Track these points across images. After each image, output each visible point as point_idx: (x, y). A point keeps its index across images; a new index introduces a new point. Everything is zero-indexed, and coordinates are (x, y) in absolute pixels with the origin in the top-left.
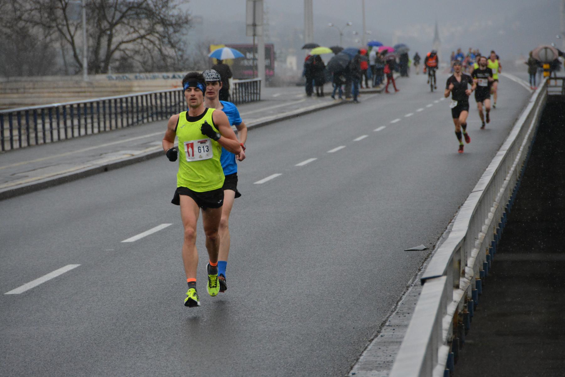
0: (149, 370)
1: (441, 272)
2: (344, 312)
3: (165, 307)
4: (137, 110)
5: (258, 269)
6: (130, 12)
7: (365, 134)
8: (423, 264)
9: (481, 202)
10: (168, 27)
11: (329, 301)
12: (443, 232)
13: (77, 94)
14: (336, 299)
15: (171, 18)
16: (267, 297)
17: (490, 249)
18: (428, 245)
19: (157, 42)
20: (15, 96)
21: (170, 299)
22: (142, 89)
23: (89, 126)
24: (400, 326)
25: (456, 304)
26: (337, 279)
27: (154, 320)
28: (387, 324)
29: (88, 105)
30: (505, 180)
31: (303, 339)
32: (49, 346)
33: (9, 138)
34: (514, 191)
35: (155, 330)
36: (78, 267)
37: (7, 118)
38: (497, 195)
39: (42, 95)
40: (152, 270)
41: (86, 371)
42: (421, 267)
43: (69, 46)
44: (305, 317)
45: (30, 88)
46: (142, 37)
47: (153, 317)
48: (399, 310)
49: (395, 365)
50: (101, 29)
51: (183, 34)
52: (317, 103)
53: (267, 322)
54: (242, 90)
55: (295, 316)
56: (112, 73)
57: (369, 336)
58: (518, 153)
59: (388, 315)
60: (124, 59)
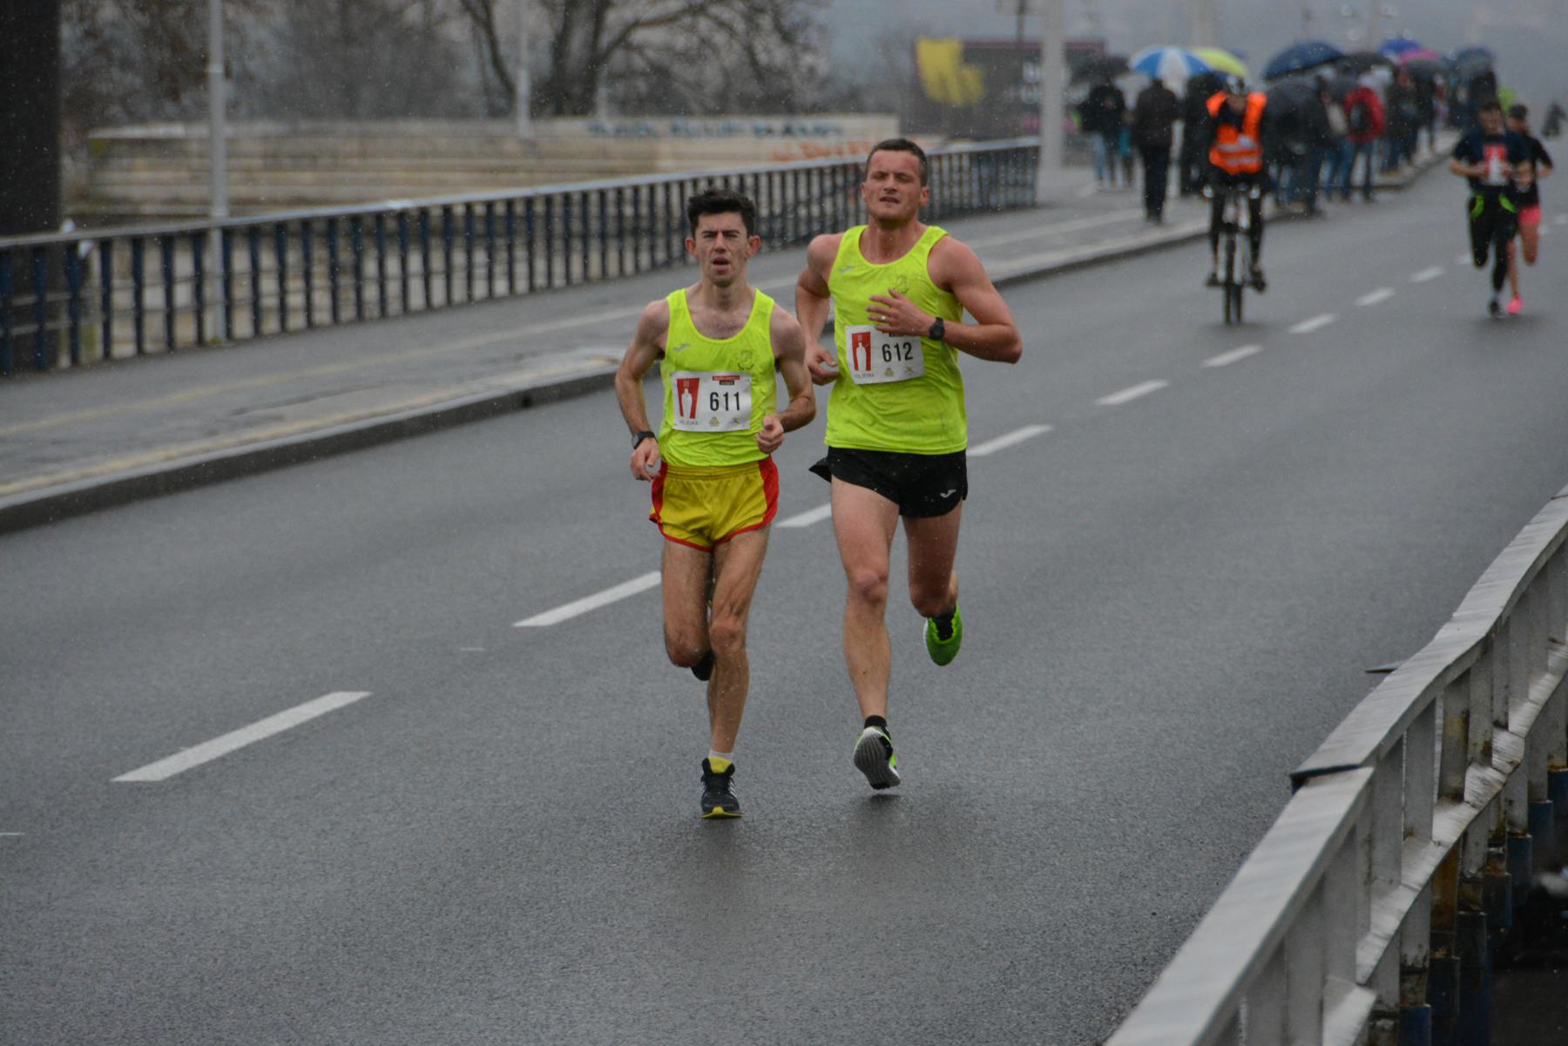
0: (487, 1033)
4: (668, 225)
20: (307, 176)
21: (613, 809)
23: (480, 272)
27: (547, 873)
29: (519, 209)
35: (541, 904)
36: (362, 701)
41: (289, 1035)
47: (547, 864)
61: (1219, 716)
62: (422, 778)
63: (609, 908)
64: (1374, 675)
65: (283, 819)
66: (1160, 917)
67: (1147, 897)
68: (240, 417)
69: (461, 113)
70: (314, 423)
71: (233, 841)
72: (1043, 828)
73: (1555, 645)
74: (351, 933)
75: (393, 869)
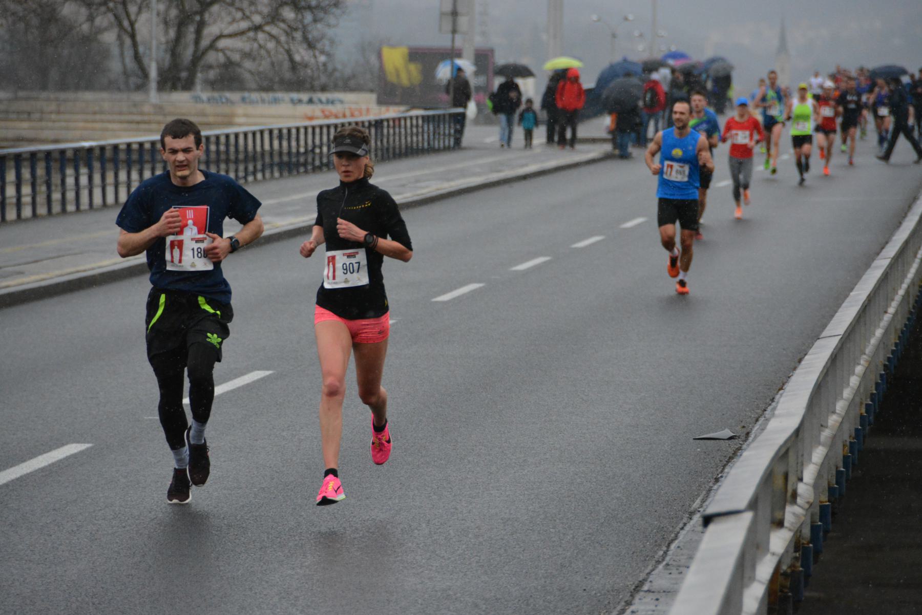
1: (743, 504)
2: (570, 557)
3: (237, 535)
5: (418, 466)
8: (723, 469)
9: (834, 359)
10: (303, 11)
11: (544, 533)
12: (767, 408)
13: (134, 126)
14: (557, 530)
16: (429, 520)
17: (850, 442)
18: (739, 431)
19: (283, 38)
20: (25, 125)
21: (247, 519)
24: (669, 592)
26: (563, 491)
28: (646, 588)
30: (886, 312)
31: (487, 608)
32: (5, 605)
33: (14, 200)
34: (902, 332)
36: (87, 449)
37: (12, 164)
38: (869, 342)
39: (72, 125)
40: (222, 459)
42: (720, 475)
44: (496, 563)
45: (51, 113)
46: (257, 28)
48: (670, 560)
51: (329, 26)
53: (422, 572)
54: (429, 129)
55: (477, 562)
56: (202, 91)
57: (612, 608)
58: (914, 261)
59: (650, 568)
61: (608, 465)
62: (130, 498)
63: (252, 582)
64: (698, 441)
65: (47, 523)
66: (588, 592)
69: (111, 86)
71: (18, 537)
72: (510, 535)
73: (823, 428)
74: (96, 596)
75: (118, 556)
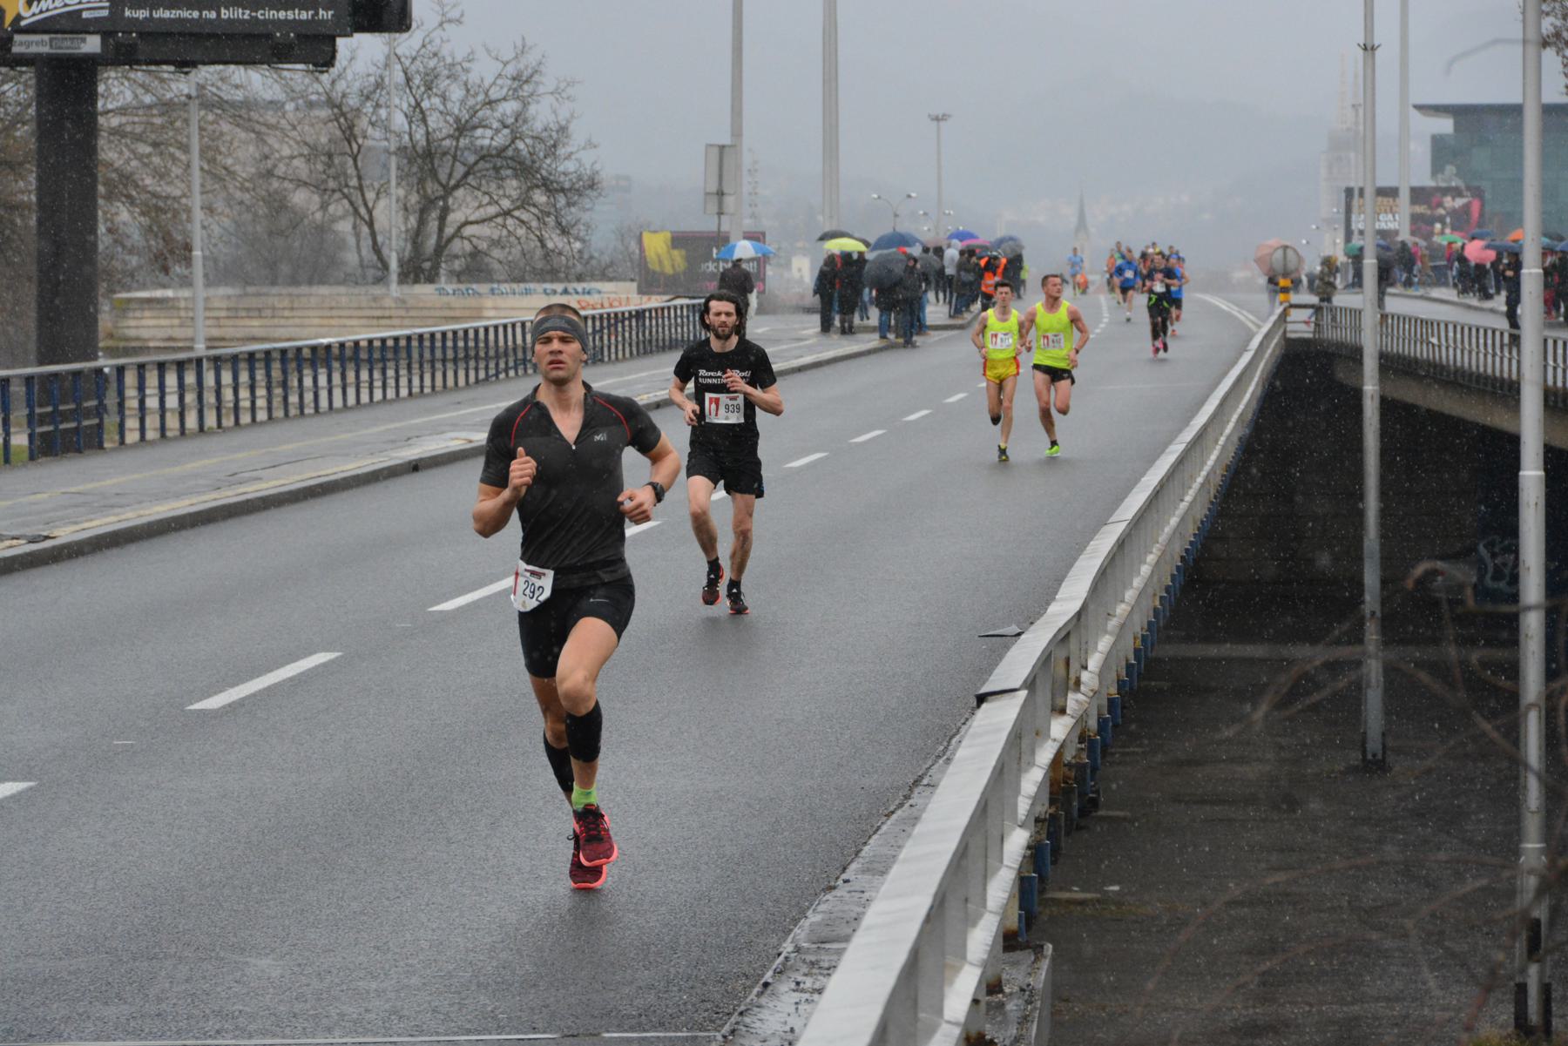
6: (482, 165)
7: (927, 409)
9: (1121, 544)
13: (375, 322)
15: (562, 178)
17: (1143, 636)
19: (534, 224)
20: (255, 323)
22: (502, 314)
25: (1056, 746)
28: (925, 782)
30: (1182, 500)
33: (231, 405)
34: (1202, 522)
39: (306, 321)
43: (365, 230)
45: (284, 309)
46: (507, 213)
49: (895, 870)
50: (425, 196)
51: (585, 210)
52: (842, 346)
56: (446, 283)
58: (1215, 448)
59: (930, 763)
60: (476, 254)
67: (857, 777)
68: (234, 478)
69: (348, 280)
70: (282, 482)
